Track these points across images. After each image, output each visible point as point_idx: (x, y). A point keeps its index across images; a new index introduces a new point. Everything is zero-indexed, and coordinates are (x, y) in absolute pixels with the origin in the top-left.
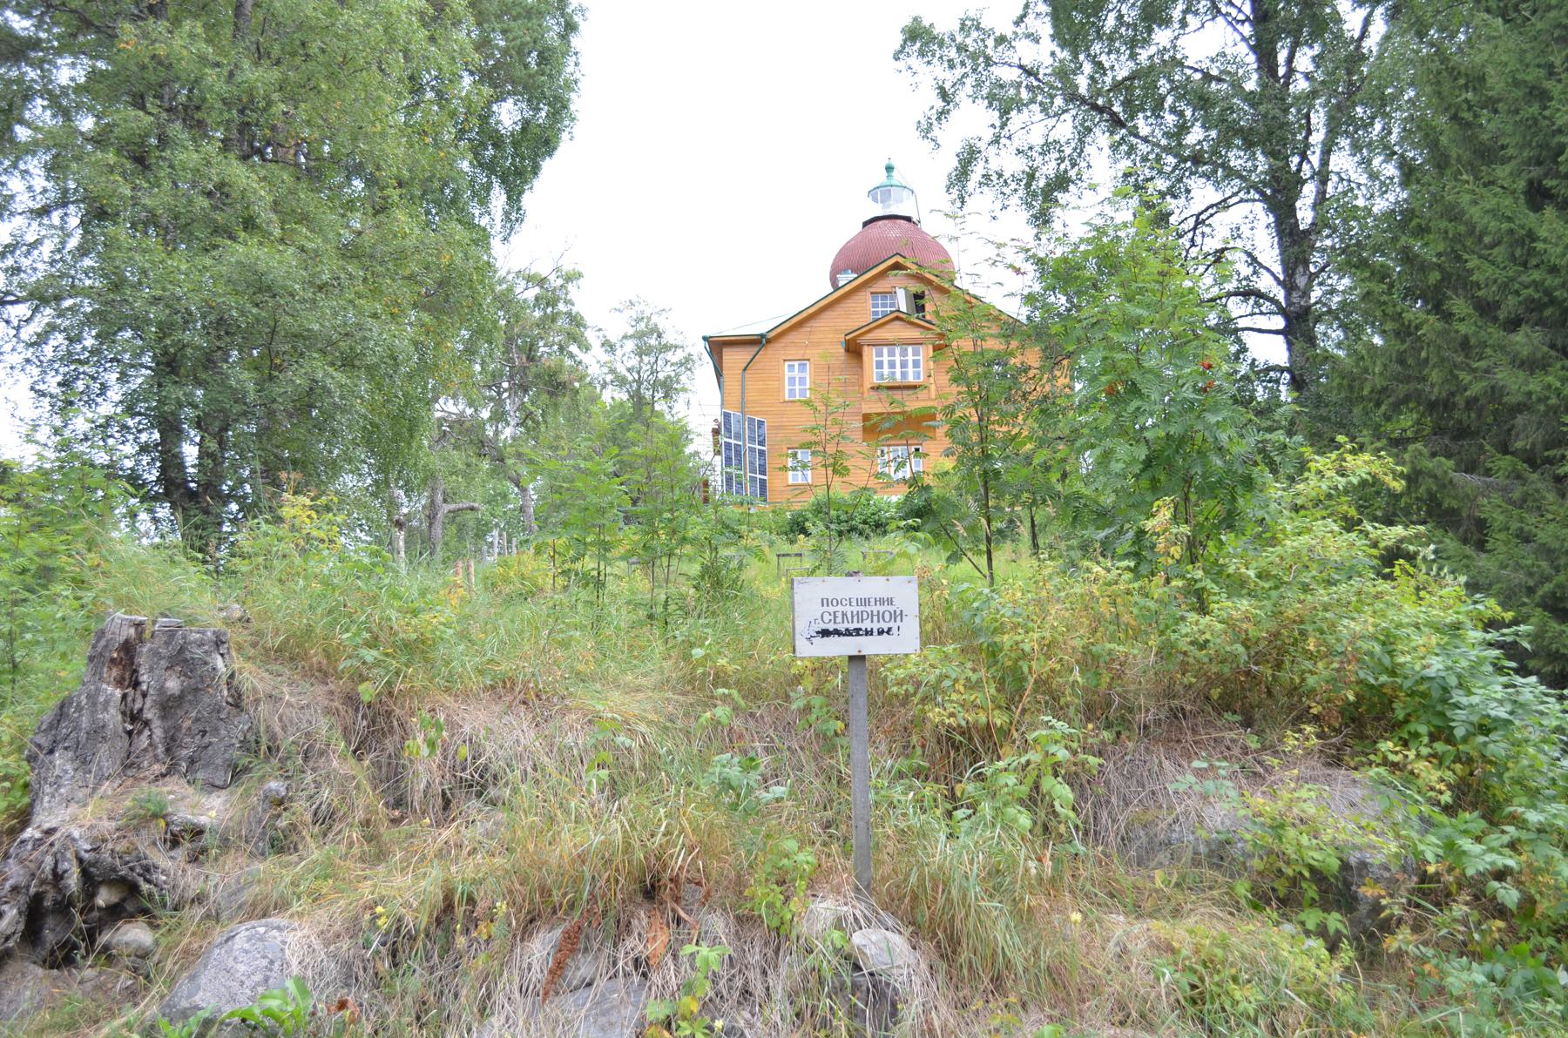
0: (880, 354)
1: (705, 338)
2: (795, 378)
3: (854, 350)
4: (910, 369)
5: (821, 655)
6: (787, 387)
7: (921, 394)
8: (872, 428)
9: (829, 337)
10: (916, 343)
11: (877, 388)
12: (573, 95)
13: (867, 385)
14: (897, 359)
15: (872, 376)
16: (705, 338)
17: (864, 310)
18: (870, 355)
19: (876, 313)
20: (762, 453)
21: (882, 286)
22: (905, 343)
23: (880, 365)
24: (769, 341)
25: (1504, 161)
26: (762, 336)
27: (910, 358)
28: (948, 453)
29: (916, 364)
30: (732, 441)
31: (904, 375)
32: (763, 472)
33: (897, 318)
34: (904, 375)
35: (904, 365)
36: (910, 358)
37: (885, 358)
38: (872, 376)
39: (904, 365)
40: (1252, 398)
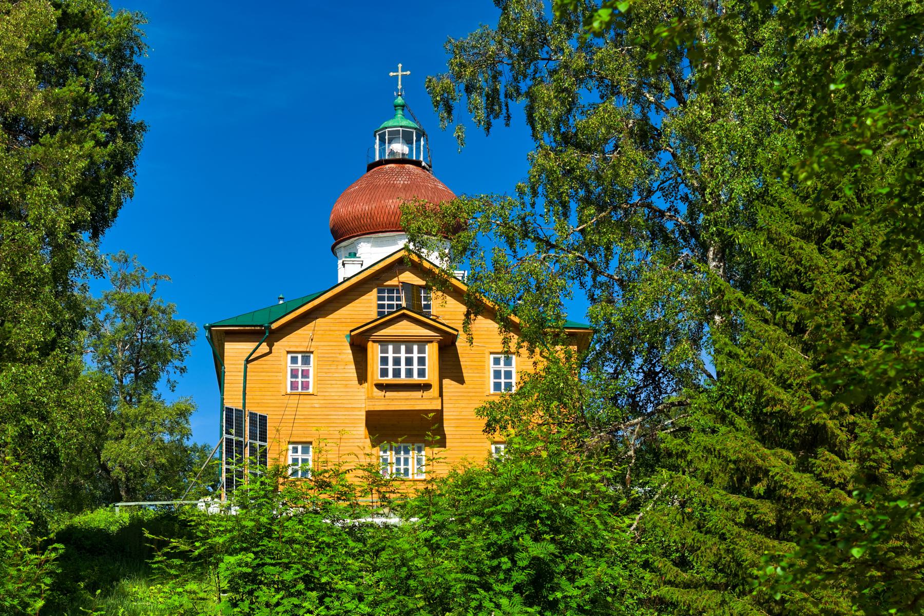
23: (384, 361)
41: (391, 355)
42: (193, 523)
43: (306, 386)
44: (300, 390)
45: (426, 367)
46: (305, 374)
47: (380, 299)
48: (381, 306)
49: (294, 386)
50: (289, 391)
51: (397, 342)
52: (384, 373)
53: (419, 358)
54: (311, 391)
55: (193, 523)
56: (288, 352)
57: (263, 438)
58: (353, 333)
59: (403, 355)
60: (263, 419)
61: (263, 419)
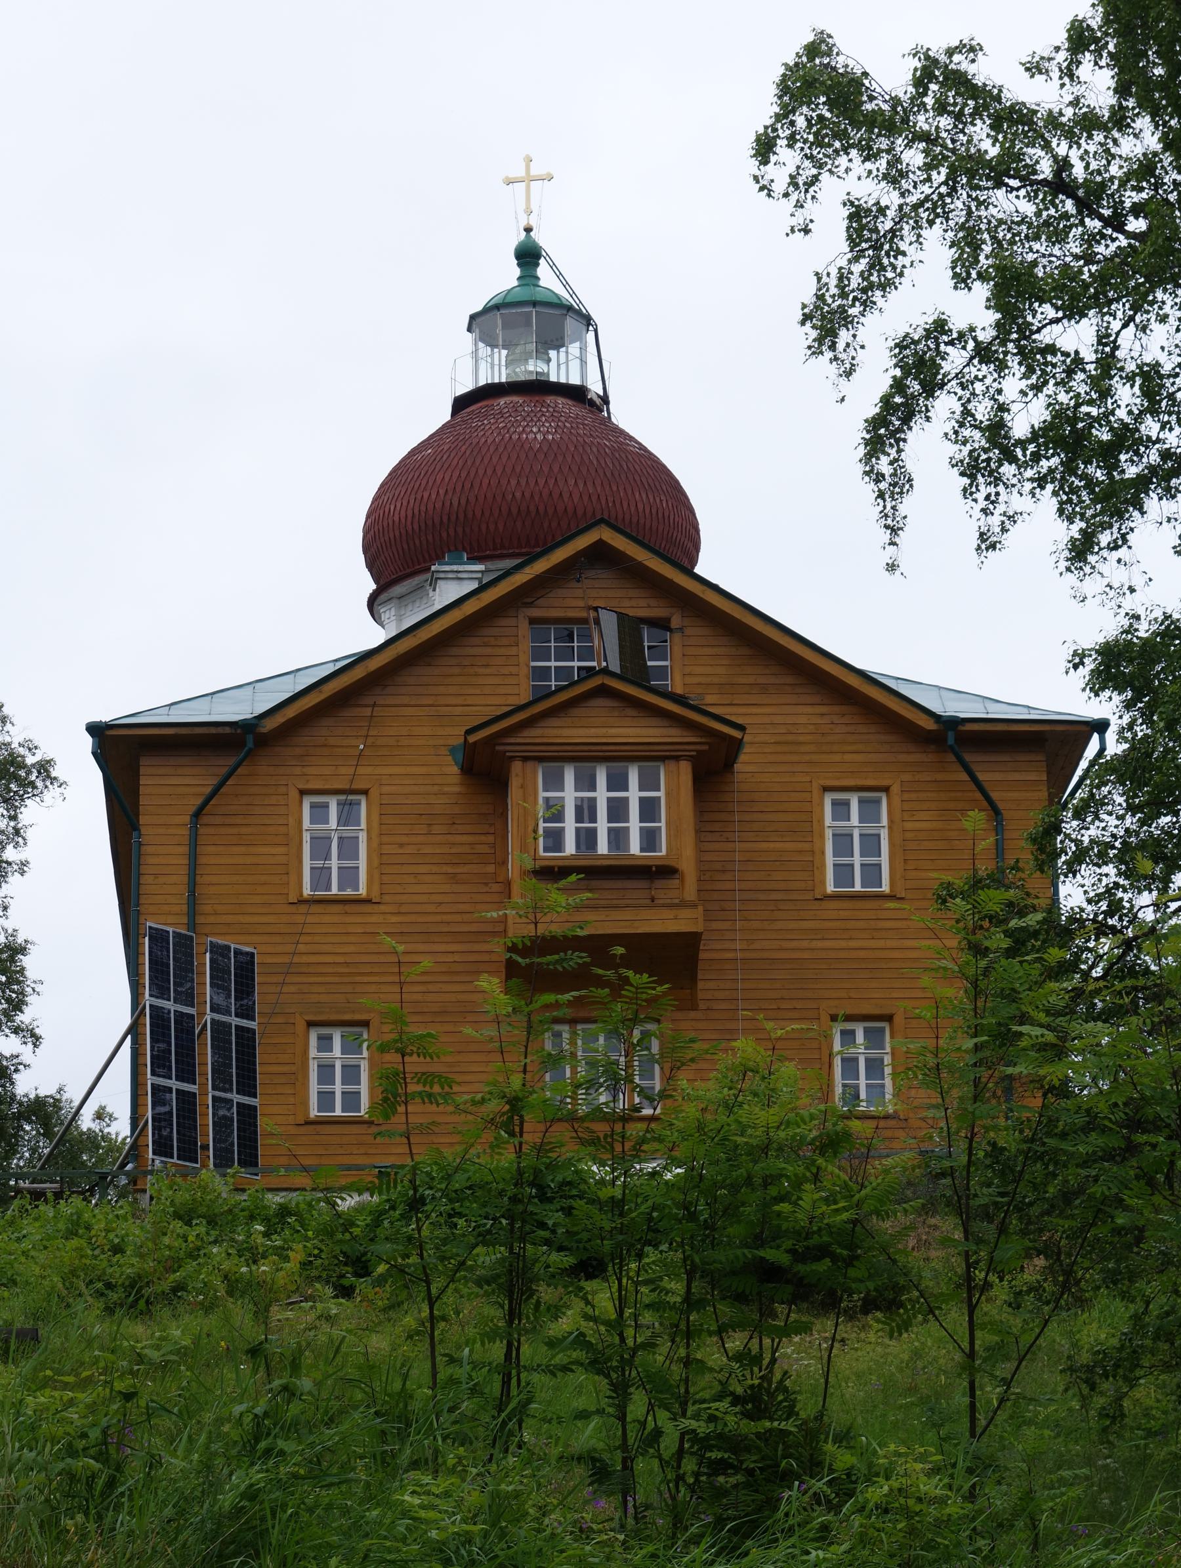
2: (333, 844)
3: (487, 768)
4: (634, 825)
5: (692, 833)
7: (666, 890)
8: (538, 968)
9: (420, 748)
10: (649, 756)
12: (1006, 94)
13: (517, 862)
14: (602, 795)
16: (95, 729)
17: (504, 677)
19: (543, 673)
21: (566, 602)
22: (616, 757)
27: (634, 794)
29: (649, 809)
31: (618, 838)
33: (603, 691)
34: (618, 838)
35: (618, 810)
36: (634, 794)
39: (618, 810)
40: (996, 126)
44: (335, 890)
58: (472, 739)
61: (246, 965)
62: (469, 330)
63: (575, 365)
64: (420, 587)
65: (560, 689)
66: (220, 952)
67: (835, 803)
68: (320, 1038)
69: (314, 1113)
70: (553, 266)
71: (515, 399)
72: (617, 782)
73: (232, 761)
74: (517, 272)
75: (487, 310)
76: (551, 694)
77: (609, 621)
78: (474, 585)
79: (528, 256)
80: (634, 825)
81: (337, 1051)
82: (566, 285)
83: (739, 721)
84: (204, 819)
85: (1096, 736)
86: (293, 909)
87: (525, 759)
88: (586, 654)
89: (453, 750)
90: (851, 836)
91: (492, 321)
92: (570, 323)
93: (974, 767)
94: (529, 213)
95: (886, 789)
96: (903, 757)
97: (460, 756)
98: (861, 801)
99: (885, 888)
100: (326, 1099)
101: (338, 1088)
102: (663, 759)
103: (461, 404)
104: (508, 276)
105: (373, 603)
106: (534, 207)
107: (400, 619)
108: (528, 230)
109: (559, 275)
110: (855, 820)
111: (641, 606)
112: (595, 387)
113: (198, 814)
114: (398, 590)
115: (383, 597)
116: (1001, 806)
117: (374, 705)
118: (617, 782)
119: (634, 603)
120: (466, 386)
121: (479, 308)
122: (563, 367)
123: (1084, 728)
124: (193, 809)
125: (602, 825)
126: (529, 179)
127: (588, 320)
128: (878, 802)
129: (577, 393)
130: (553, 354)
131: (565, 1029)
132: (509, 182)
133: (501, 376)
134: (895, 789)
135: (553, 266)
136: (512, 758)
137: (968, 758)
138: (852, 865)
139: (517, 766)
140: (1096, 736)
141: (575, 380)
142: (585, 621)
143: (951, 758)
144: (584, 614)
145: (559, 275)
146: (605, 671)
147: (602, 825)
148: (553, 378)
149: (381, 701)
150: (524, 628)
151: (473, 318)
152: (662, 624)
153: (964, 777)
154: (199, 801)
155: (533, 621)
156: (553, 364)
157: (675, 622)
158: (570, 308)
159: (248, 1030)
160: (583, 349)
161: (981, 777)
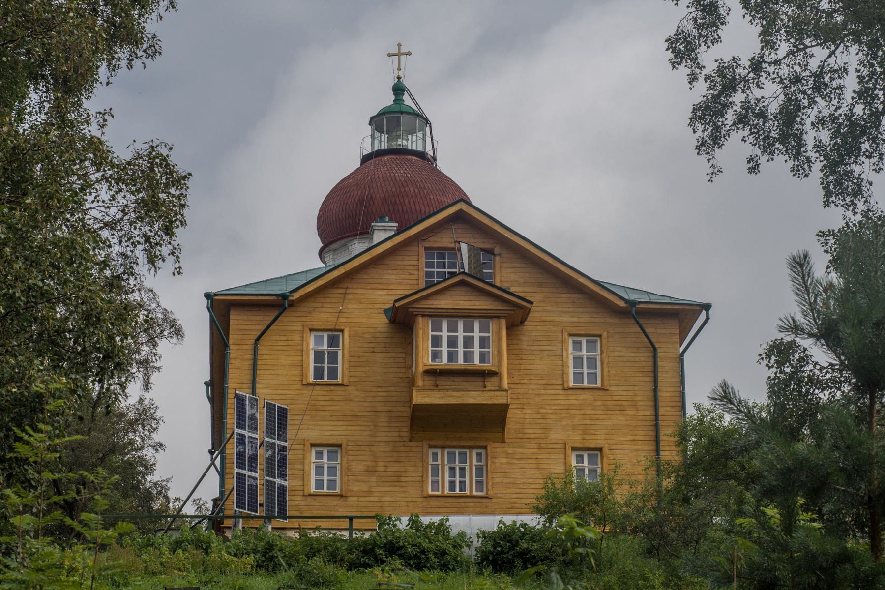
0: (437, 328)
1: (208, 296)
4: (477, 350)
6: (571, 370)
7: (491, 383)
10: (485, 316)
11: (431, 373)
15: (425, 359)
16: (208, 296)
18: (424, 330)
19: (429, 275)
20: (284, 449)
21: (444, 240)
22: (468, 315)
23: (436, 341)
24: (292, 304)
25: (802, 506)
26: (284, 296)
28: (730, 424)
30: (246, 433)
31: (468, 357)
32: (283, 476)
33: (462, 283)
35: (468, 342)
36: (477, 335)
37: (445, 334)
38: (425, 359)
39: (468, 342)
41: (461, 334)
42: (417, 191)
43: (333, 373)
44: (326, 379)
45: (430, 349)
46: (333, 358)
47: (429, 265)
48: (429, 275)
49: (318, 373)
50: (311, 379)
51: (453, 315)
52: (436, 355)
53: (480, 337)
54: (339, 380)
55: (417, 191)
56: (312, 445)
57: (282, 436)
58: (397, 305)
59: (461, 334)
60: (283, 412)
61: (283, 412)
62: (370, 124)
63: (420, 142)
64: (345, 245)
65: (438, 283)
66: (270, 407)
67: (574, 342)
68: (317, 453)
69: (313, 490)
70: (410, 95)
71: (392, 157)
72: (469, 328)
73: (276, 313)
74: (393, 97)
75: (379, 115)
76: (436, 284)
77: (464, 247)
78: (393, 233)
79: (399, 90)
80: (477, 350)
81: (584, 351)
82: (417, 104)
83: (531, 299)
84: (260, 342)
85: (704, 312)
86: (305, 388)
87: (423, 316)
88: (453, 265)
89: (386, 311)
90: (582, 359)
91: (380, 122)
92: (418, 122)
93: (644, 326)
94: (399, 69)
95: (600, 336)
96: (610, 320)
97: (390, 314)
98: (587, 341)
99: (599, 385)
100: (319, 483)
101: (326, 478)
102: (491, 317)
103: (365, 159)
104: (389, 99)
105: (321, 253)
106: (402, 67)
107: (334, 259)
108: (399, 78)
109: (413, 100)
110: (584, 351)
111: (481, 243)
112: (431, 153)
113: (258, 339)
114: (334, 246)
115: (327, 249)
116: (657, 346)
117: (347, 288)
118: (469, 328)
119: (476, 241)
120: (368, 150)
121: (375, 114)
122: (412, 143)
123: (697, 308)
124: (256, 337)
125: (461, 350)
126: (399, 54)
127: (427, 121)
128: (596, 342)
129: (422, 155)
130: (410, 137)
131: (439, 451)
132: (390, 55)
133: (384, 146)
134: (605, 335)
135: (410, 95)
136: (417, 315)
137: (641, 321)
138: (582, 373)
139: (420, 320)
140: (704, 312)
141: (420, 149)
142: (453, 249)
143: (633, 321)
144: (452, 245)
145: (413, 100)
146: (464, 273)
147: (461, 350)
148: (409, 148)
149: (350, 286)
150: (422, 252)
151: (372, 118)
152: (490, 252)
153: (639, 330)
154: (259, 333)
155: (426, 249)
156: (410, 141)
157: (497, 250)
158: (418, 115)
159: (239, 468)
160: (425, 134)
161: (647, 330)
